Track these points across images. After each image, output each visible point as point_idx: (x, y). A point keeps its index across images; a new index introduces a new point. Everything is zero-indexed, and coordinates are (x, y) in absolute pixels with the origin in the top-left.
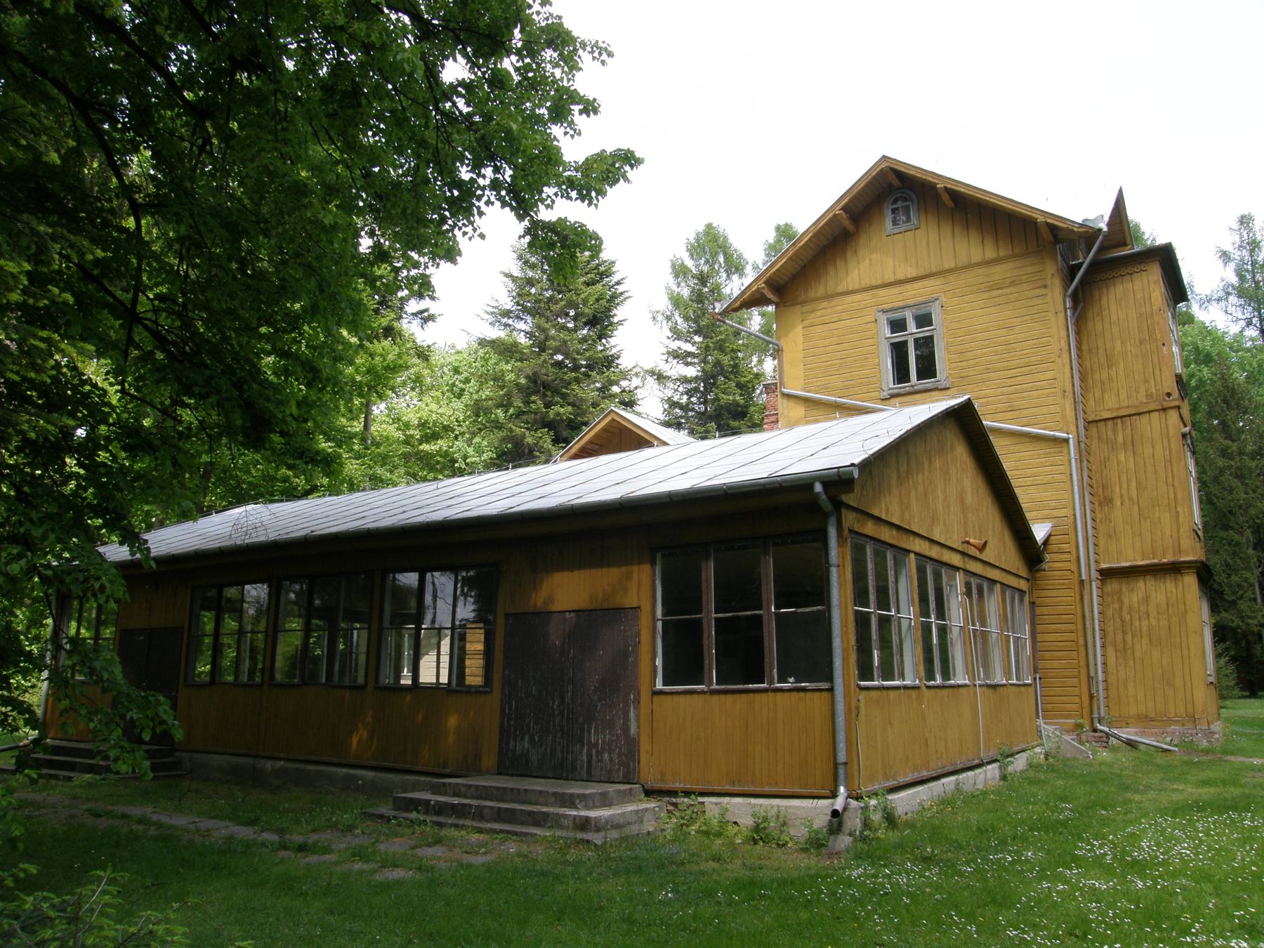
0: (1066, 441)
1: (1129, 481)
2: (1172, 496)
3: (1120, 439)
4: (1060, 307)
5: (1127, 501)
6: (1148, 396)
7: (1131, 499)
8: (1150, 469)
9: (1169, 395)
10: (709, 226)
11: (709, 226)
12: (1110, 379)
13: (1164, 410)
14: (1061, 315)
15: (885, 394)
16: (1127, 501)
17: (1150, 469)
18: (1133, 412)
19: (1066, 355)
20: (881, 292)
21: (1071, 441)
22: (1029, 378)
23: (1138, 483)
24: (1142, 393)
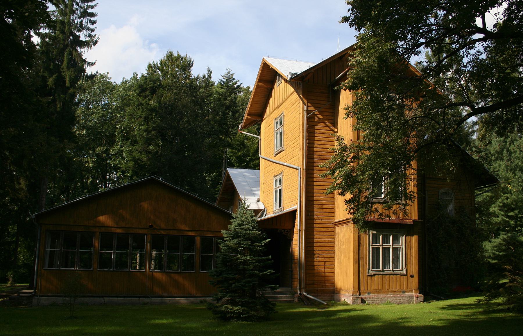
0: (298, 169)
20: (276, 111)
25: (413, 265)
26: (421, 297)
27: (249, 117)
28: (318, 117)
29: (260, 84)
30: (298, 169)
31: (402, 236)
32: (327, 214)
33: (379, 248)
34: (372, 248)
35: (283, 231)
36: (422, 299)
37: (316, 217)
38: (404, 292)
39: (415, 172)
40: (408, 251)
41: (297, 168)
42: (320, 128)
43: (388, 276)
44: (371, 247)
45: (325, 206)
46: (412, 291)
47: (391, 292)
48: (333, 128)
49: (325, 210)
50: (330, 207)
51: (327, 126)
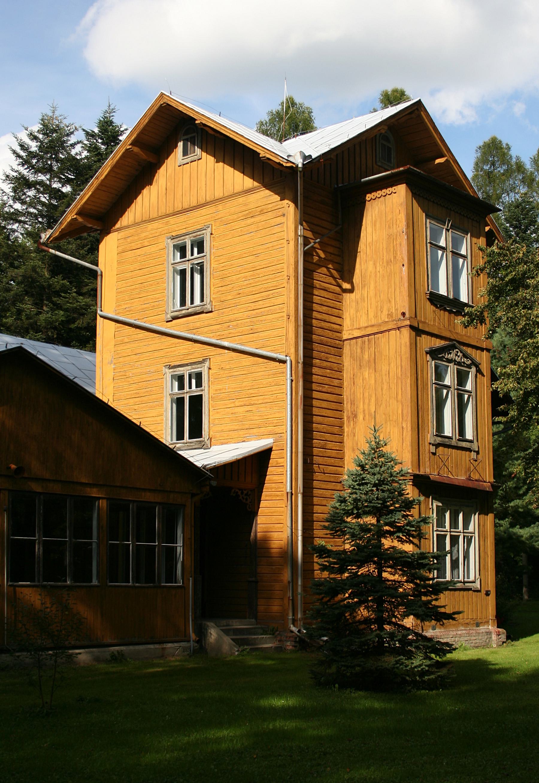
0: (284, 362)
1: (370, 396)
2: (400, 412)
3: (366, 357)
4: (292, 235)
5: (367, 416)
6: (390, 315)
7: (370, 414)
8: (385, 387)
9: (403, 314)
10: (291, 103)
11: (291, 103)
12: (363, 299)
13: (399, 328)
14: (292, 243)
15: (169, 317)
16: (367, 416)
17: (385, 387)
18: (375, 330)
19: (292, 281)
20: (171, 220)
21: (288, 362)
22: (267, 303)
23: (377, 400)
24: (385, 312)
25: (488, 571)
26: (503, 633)
27: (80, 219)
28: (318, 255)
29: (136, 149)
30: (284, 362)
31: (475, 514)
32: (332, 460)
33: (446, 535)
34: (437, 535)
35: (240, 493)
36: (503, 637)
37: (315, 467)
38: (478, 625)
39: (315, 361)
40: (482, 543)
41: (282, 357)
42: (321, 277)
43: (457, 593)
44: (435, 533)
45: (330, 445)
46: (487, 622)
47: (462, 625)
48: (340, 281)
49: (329, 453)
50: (336, 446)
51: (332, 276)
